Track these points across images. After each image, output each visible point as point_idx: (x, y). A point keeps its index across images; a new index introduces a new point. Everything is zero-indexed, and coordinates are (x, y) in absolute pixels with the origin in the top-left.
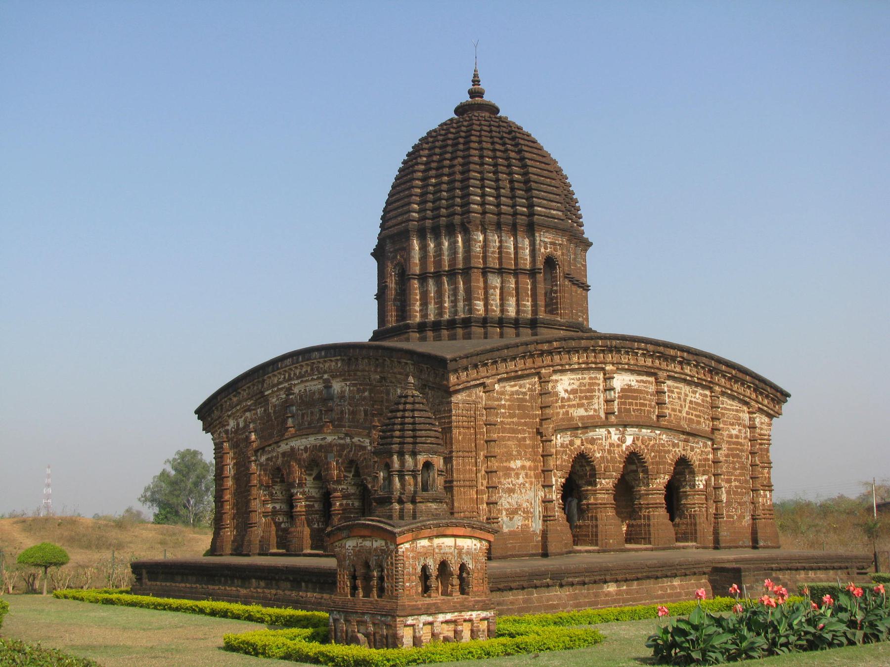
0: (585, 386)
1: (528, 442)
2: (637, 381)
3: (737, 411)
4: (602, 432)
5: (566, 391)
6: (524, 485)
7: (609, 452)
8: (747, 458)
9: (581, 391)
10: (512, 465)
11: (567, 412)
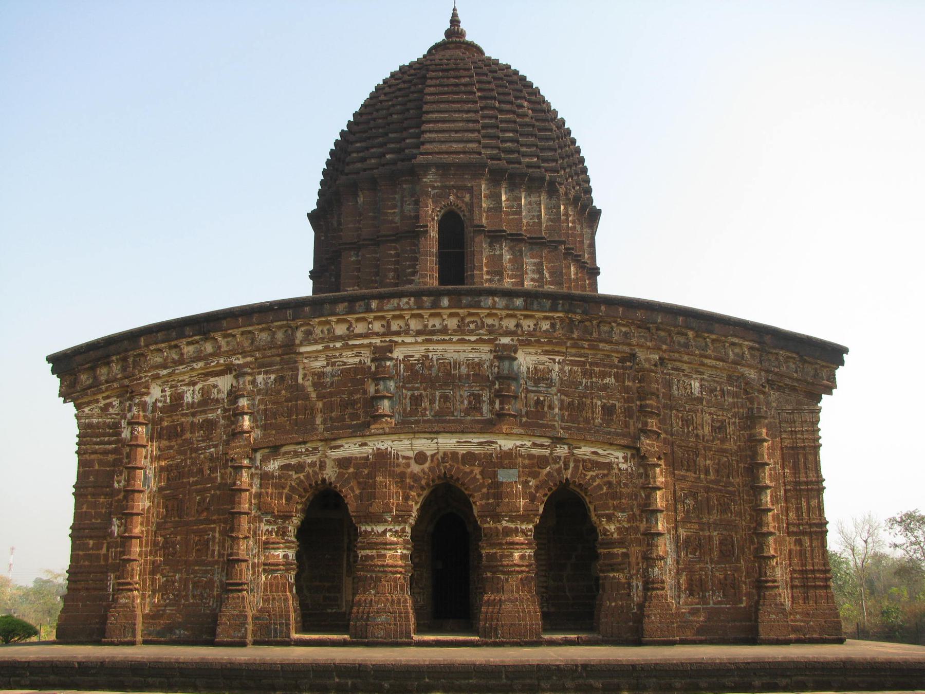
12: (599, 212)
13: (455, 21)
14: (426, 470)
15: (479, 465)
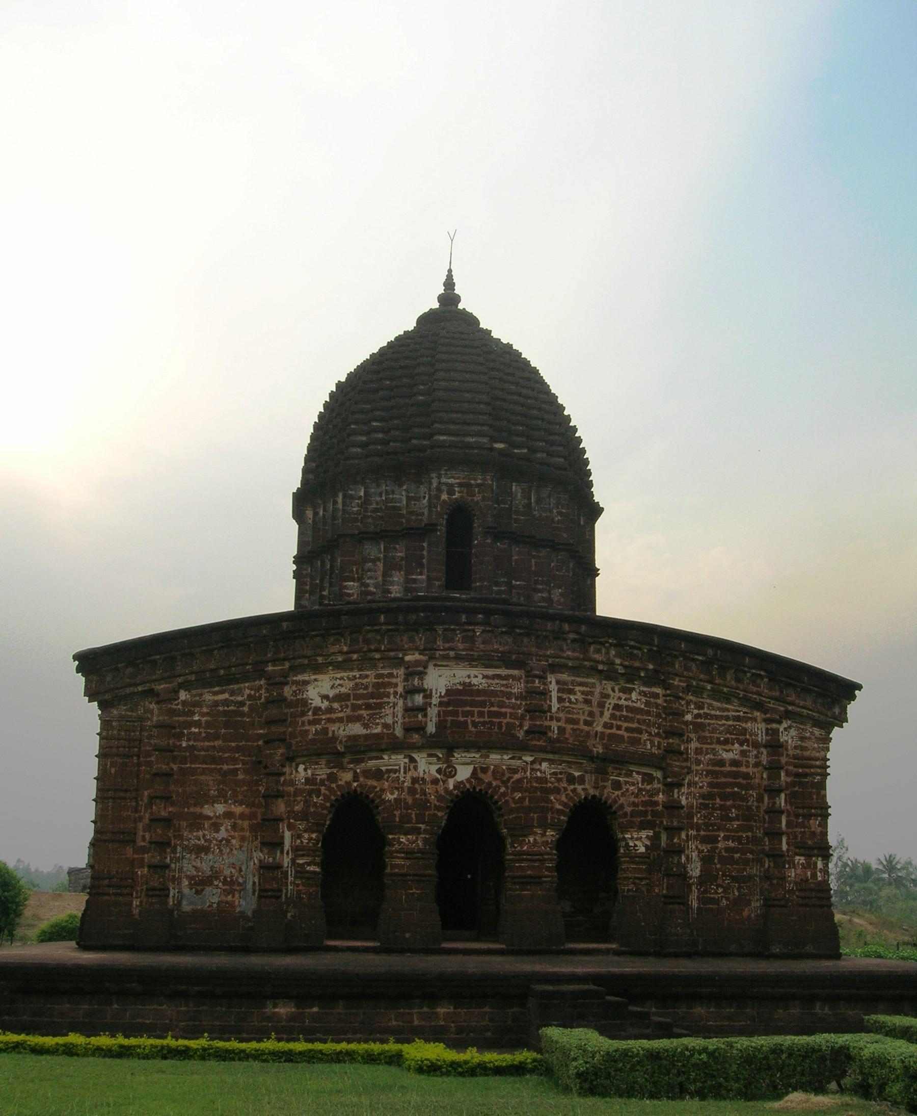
0: (366, 688)
1: (241, 777)
2: (484, 677)
3: (738, 719)
4: (400, 760)
5: (325, 697)
6: (228, 841)
7: (412, 791)
8: (760, 799)
9: (357, 697)
10: (207, 810)
11: (325, 731)
12: (601, 510)
13: (449, 284)
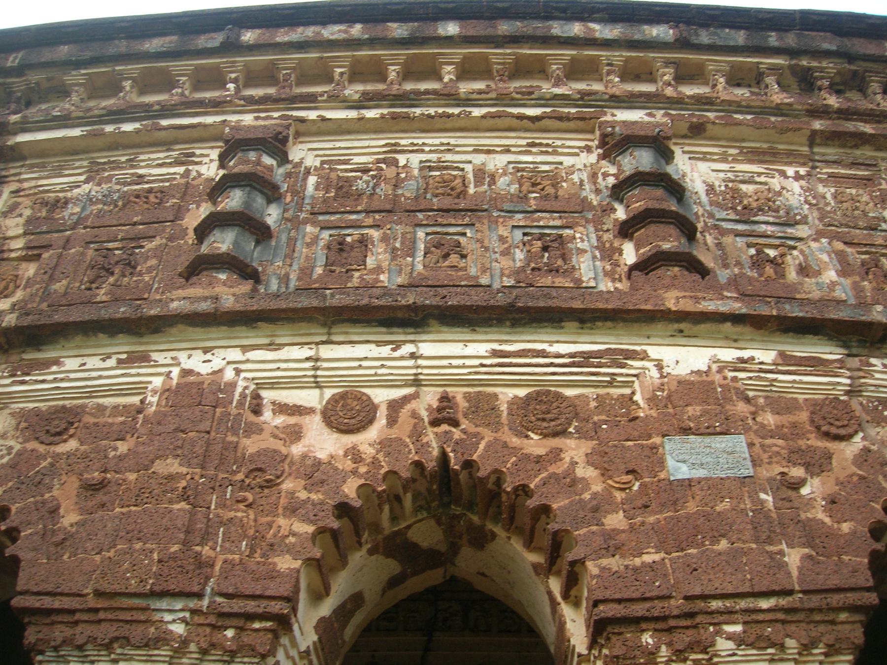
14: (368, 451)
15: (582, 435)
